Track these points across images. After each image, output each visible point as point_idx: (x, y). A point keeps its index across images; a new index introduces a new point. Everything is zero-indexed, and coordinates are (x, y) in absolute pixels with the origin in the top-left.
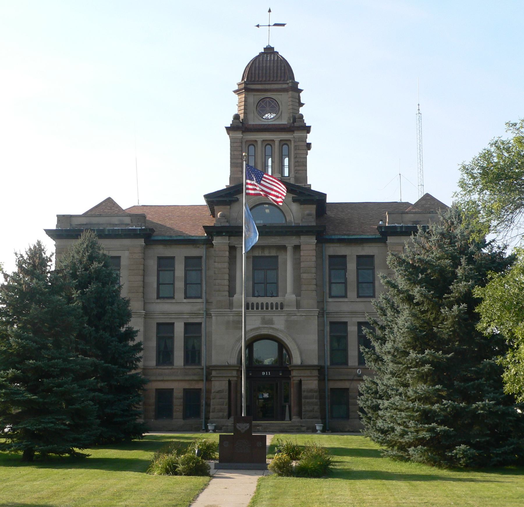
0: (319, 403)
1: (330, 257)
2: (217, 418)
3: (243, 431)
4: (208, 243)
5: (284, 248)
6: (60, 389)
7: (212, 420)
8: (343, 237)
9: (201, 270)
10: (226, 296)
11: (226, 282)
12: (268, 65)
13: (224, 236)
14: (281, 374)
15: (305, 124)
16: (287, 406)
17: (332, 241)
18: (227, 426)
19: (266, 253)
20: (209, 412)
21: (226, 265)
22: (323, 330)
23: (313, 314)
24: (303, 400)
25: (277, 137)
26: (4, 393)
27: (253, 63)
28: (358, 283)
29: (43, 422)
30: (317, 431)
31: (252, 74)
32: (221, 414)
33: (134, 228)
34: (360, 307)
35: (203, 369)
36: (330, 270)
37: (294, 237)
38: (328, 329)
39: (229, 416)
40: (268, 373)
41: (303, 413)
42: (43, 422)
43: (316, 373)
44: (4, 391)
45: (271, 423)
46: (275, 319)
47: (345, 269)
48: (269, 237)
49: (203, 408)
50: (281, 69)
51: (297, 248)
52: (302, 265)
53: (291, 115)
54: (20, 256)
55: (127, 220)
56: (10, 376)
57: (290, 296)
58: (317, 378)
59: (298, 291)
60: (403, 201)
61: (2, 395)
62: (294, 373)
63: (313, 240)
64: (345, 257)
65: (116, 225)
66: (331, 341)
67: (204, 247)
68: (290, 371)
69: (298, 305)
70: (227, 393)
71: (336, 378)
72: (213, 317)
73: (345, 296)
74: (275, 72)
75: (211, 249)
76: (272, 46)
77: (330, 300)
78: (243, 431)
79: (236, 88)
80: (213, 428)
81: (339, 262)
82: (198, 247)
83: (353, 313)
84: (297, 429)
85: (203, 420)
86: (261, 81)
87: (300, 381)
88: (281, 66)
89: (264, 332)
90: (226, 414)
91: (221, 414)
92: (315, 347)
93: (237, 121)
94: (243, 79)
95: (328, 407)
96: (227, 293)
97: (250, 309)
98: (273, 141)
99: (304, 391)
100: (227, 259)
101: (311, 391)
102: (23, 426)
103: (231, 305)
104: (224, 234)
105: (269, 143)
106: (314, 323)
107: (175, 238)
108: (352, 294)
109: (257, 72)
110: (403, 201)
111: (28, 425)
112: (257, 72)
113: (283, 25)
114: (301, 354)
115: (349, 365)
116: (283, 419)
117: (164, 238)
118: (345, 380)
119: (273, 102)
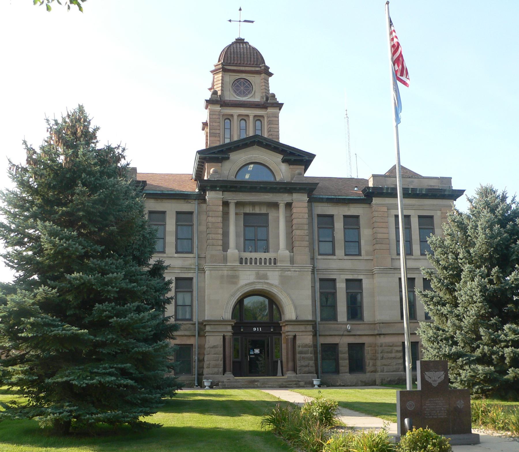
0: (314, 358)
1: (319, 216)
2: (212, 374)
3: (435, 384)
4: (201, 198)
5: (275, 205)
6: (122, 319)
7: (207, 376)
8: (330, 197)
9: (192, 225)
10: (220, 250)
11: (220, 237)
12: (242, 51)
13: (218, 190)
14: (272, 330)
16: (279, 362)
17: (321, 200)
18: (223, 382)
19: (257, 210)
20: (203, 368)
21: (220, 219)
22: (314, 287)
23: (307, 270)
24: (298, 356)
25: (252, 112)
26: (32, 324)
27: (228, 49)
29: (97, 374)
30: (314, 386)
32: (216, 370)
34: (348, 264)
35: (195, 324)
36: (319, 228)
38: (318, 285)
39: (224, 371)
40: (259, 329)
41: (298, 368)
42: (97, 374)
43: (310, 328)
44: (32, 320)
45: (270, 379)
46: (269, 274)
47: (333, 228)
48: (262, 194)
49: (196, 364)
50: (254, 55)
51: (289, 205)
52: (295, 222)
53: (264, 94)
54: (54, 122)
56: (39, 297)
57: (283, 252)
58: (311, 333)
59: (291, 246)
60: (359, 177)
61: (28, 326)
62: (285, 329)
63: (305, 198)
64: (332, 216)
66: (320, 296)
67: (196, 202)
68: (281, 327)
69: (292, 261)
70: (222, 349)
71: (327, 333)
72: (207, 272)
73: (333, 254)
74: (249, 56)
75: (203, 205)
76: (243, 38)
77: (320, 257)
78: (435, 384)
79: (213, 68)
80: (209, 384)
81: (327, 220)
82: (190, 203)
83: (342, 270)
84: (296, 384)
85: (196, 376)
86: (236, 63)
87: (295, 336)
88: (254, 53)
89: (259, 287)
90: (221, 369)
91: (216, 370)
92: (309, 302)
93: (216, 96)
94: (219, 61)
95: (319, 362)
96: (221, 248)
97: (244, 264)
98: (248, 116)
99: (299, 347)
100: (220, 214)
101: (306, 346)
102: (65, 379)
103: (225, 259)
104: (218, 189)
106: (309, 277)
107: (167, 192)
108: (340, 252)
109: (232, 56)
110: (360, 177)
111: (72, 378)
112: (232, 56)
113: (252, 22)
114: (296, 308)
116: (275, 374)
117: (155, 192)
118: (335, 335)
119: (247, 82)
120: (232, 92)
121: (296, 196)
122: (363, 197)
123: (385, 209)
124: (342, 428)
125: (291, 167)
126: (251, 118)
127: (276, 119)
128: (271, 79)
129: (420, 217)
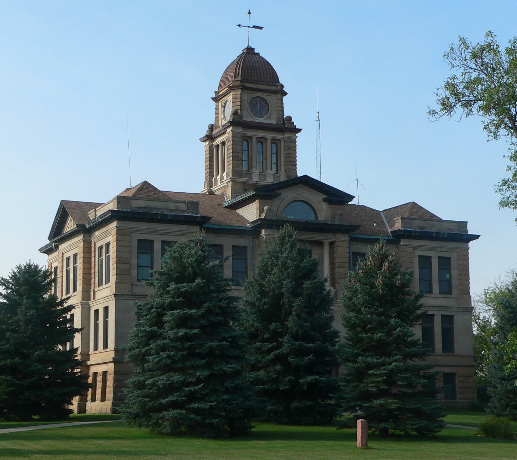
15: (295, 126)
25: (269, 135)
28: (138, 266)
31: (245, 73)
33: (190, 214)
34: (441, 301)
37: (330, 234)
51: (332, 244)
55: (183, 207)
60: (360, 204)
63: (347, 238)
65: (173, 210)
76: (252, 47)
98: (265, 139)
105: (261, 140)
107: (224, 227)
113: (261, 28)
115: (456, 352)
117: (214, 227)
120: (249, 111)
121: (339, 236)
122: (393, 238)
123: (411, 250)
124: (373, 449)
125: (332, 206)
126: (269, 142)
127: (294, 144)
128: (285, 98)
129: (439, 258)
